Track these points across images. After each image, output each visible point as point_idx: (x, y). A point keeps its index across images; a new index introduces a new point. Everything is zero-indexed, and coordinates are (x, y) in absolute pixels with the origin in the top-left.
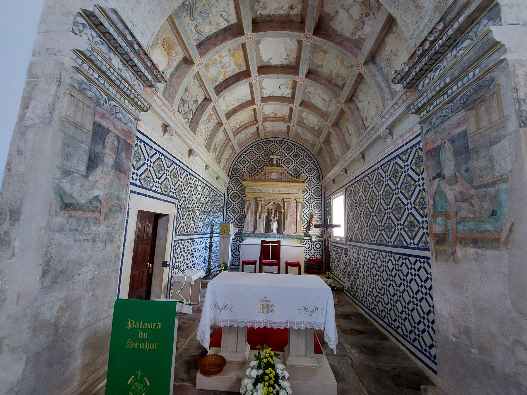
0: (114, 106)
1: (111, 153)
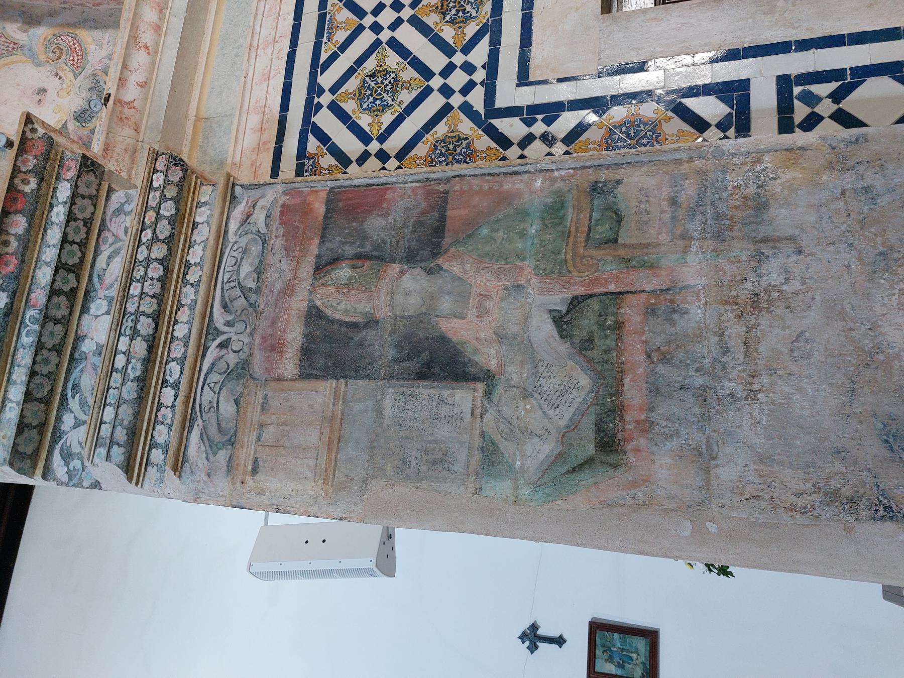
0: (225, 306)
1: (385, 286)
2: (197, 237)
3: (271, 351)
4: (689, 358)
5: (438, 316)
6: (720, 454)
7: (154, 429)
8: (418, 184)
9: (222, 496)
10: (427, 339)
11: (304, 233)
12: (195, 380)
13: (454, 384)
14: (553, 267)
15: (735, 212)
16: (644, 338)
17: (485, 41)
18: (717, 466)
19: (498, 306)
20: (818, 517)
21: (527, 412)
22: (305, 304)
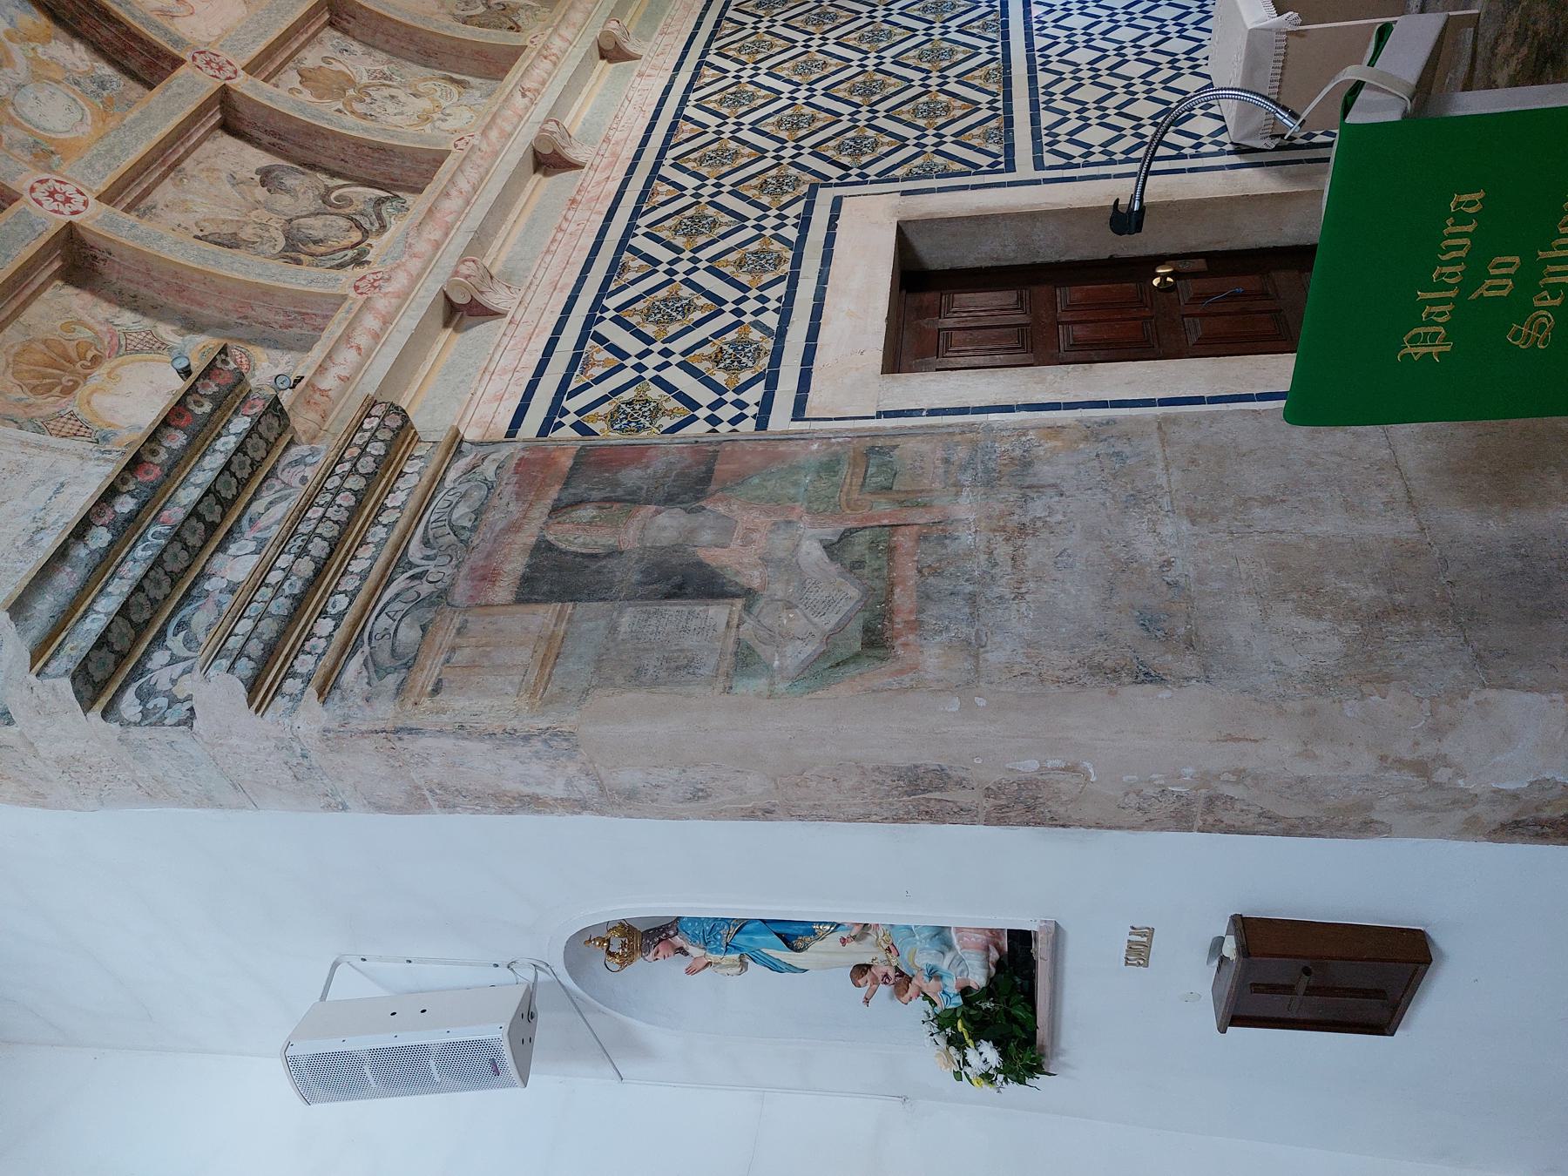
0: (426, 542)
17: (761, 385)
20: (1084, 685)
21: (790, 620)
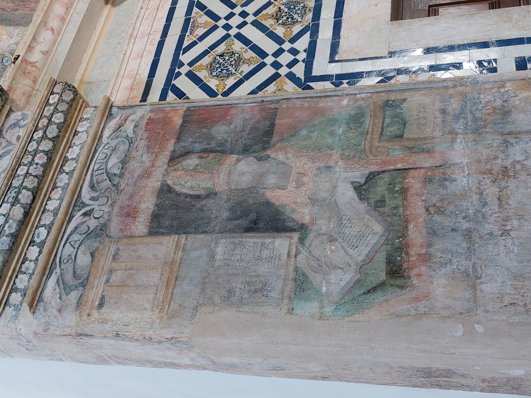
0: (92, 187)
2: (77, 141)
3: (126, 217)
4: (457, 210)
5: (265, 188)
6: (483, 274)
7: (17, 277)
8: (255, 104)
9: (69, 327)
10: (255, 204)
11: (164, 136)
12: (59, 239)
13: (275, 234)
14: (353, 154)
15: (487, 117)
16: (423, 198)
18: (482, 283)
19: (312, 182)
21: (332, 251)
22: (159, 183)
